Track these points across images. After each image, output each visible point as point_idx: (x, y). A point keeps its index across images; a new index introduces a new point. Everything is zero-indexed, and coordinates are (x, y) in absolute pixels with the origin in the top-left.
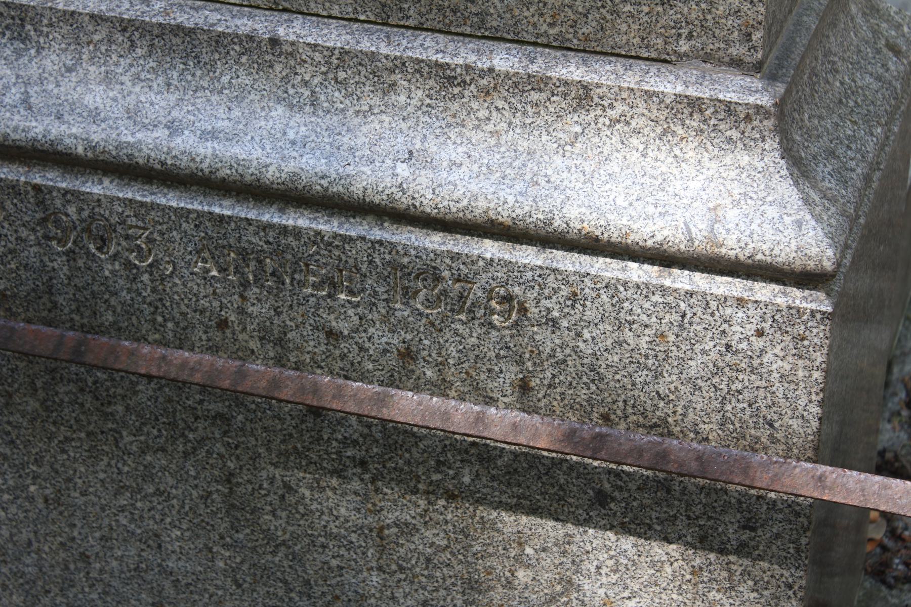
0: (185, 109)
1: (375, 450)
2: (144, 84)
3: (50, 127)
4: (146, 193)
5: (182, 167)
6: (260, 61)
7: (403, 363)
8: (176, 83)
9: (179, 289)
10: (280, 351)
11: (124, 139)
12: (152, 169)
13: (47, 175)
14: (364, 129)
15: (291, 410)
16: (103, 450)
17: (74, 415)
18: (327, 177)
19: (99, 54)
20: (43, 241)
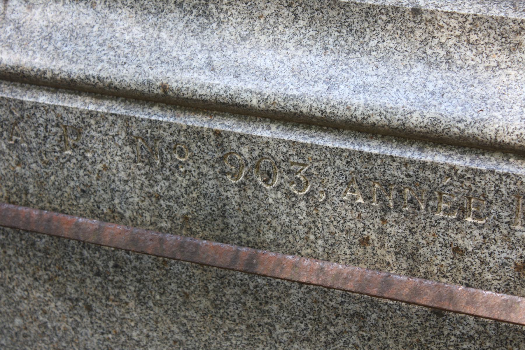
0: (340, 68)
1: (488, 344)
2: (305, 48)
3: (230, 84)
4: (306, 136)
5: (339, 114)
6: (403, 28)
7: (519, 274)
8: (331, 47)
9: (330, 213)
10: (411, 263)
11: (290, 93)
12: (314, 116)
13: (226, 123)
14: (493, 81)
15: (418, 311)
16: (259, 339)
17: (237, 311)
18: (463, 121)
19: (268, 26)
20: (220, 176)
